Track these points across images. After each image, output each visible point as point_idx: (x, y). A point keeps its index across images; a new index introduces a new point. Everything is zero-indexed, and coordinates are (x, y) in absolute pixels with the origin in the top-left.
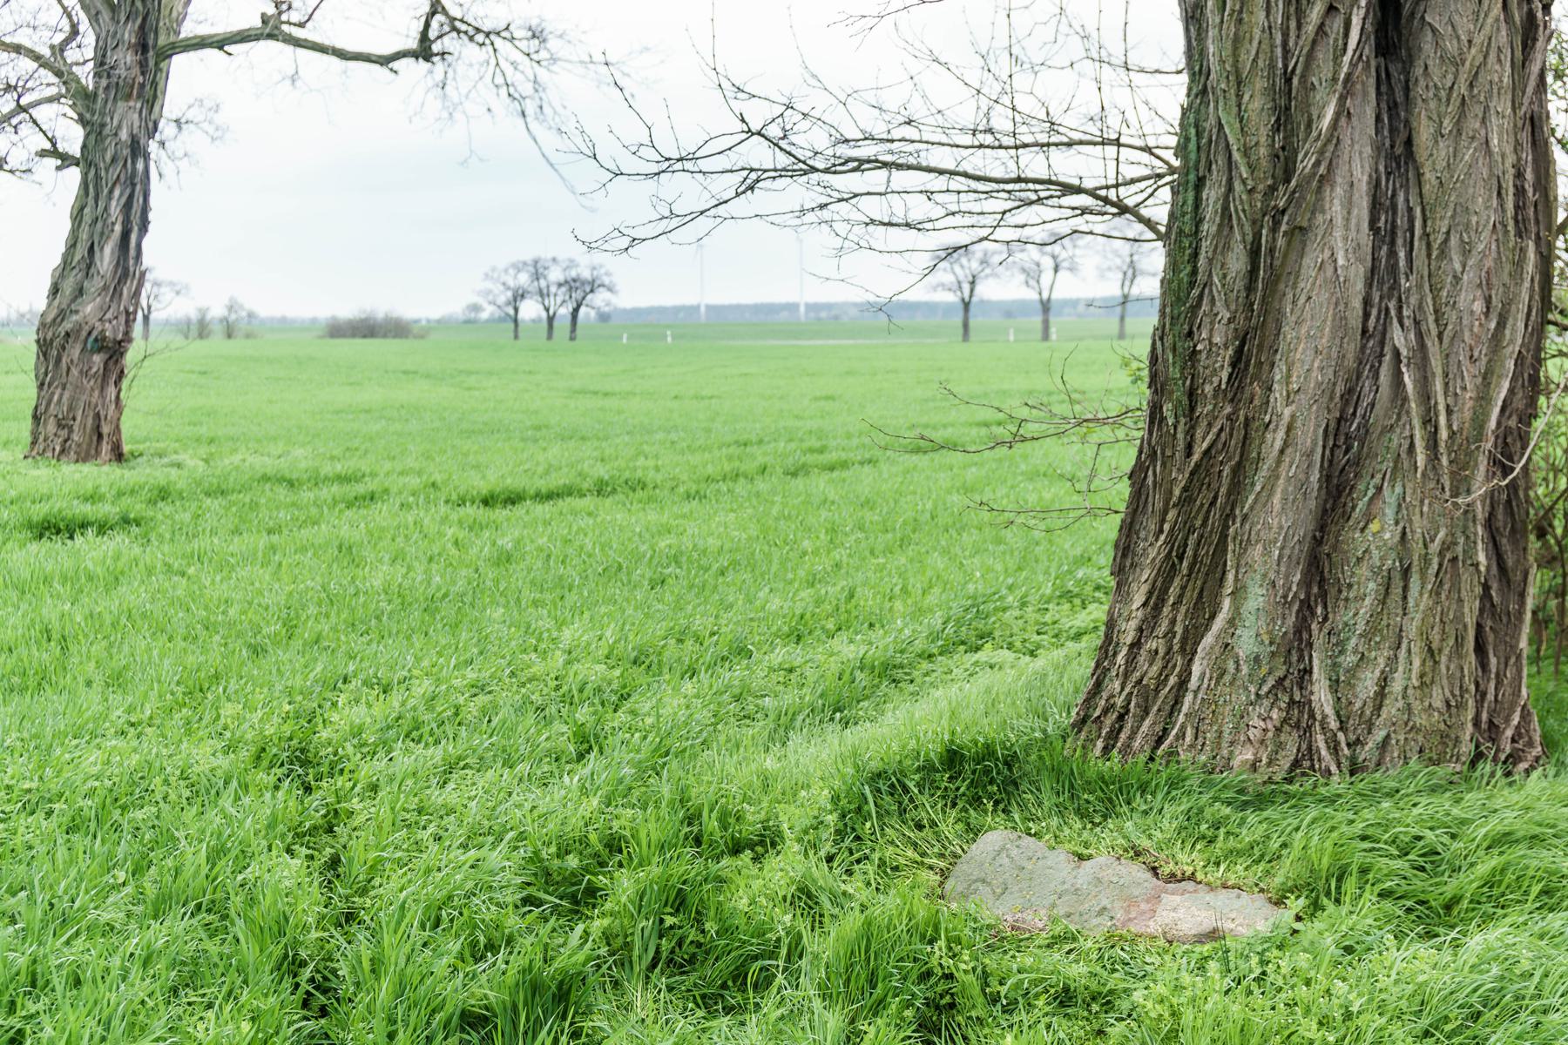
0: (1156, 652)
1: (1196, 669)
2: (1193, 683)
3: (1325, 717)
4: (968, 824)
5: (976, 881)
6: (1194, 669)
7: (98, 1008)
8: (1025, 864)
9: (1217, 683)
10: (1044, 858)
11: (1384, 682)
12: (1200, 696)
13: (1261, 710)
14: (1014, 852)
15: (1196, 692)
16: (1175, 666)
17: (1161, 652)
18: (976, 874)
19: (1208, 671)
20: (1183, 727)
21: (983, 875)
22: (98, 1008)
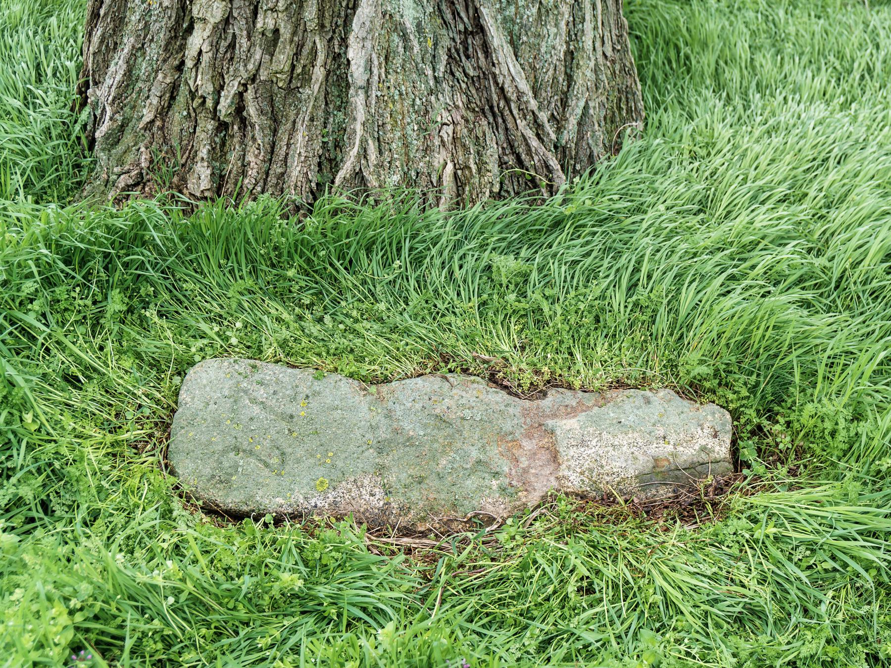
0: (276, 31)
1: (355, 54)
2: (357, 73)
3: (520, 94)
4: (138, 356)
5: (225, 452)
6: (351, 54)
7: (847, 235)
8: (291, 409)
9: (387, 73)
10: (316, 394)
11: (574, 36)
12: (374, 93)
13: (445, 98)
14: (261, 393)
15: (367, 88)
16: (314, 52)
17: (285, 32)
18: (219, 442)
19: (374, 56)
20: (364, 141)
21: (231, 441)
22: (847, 235)
